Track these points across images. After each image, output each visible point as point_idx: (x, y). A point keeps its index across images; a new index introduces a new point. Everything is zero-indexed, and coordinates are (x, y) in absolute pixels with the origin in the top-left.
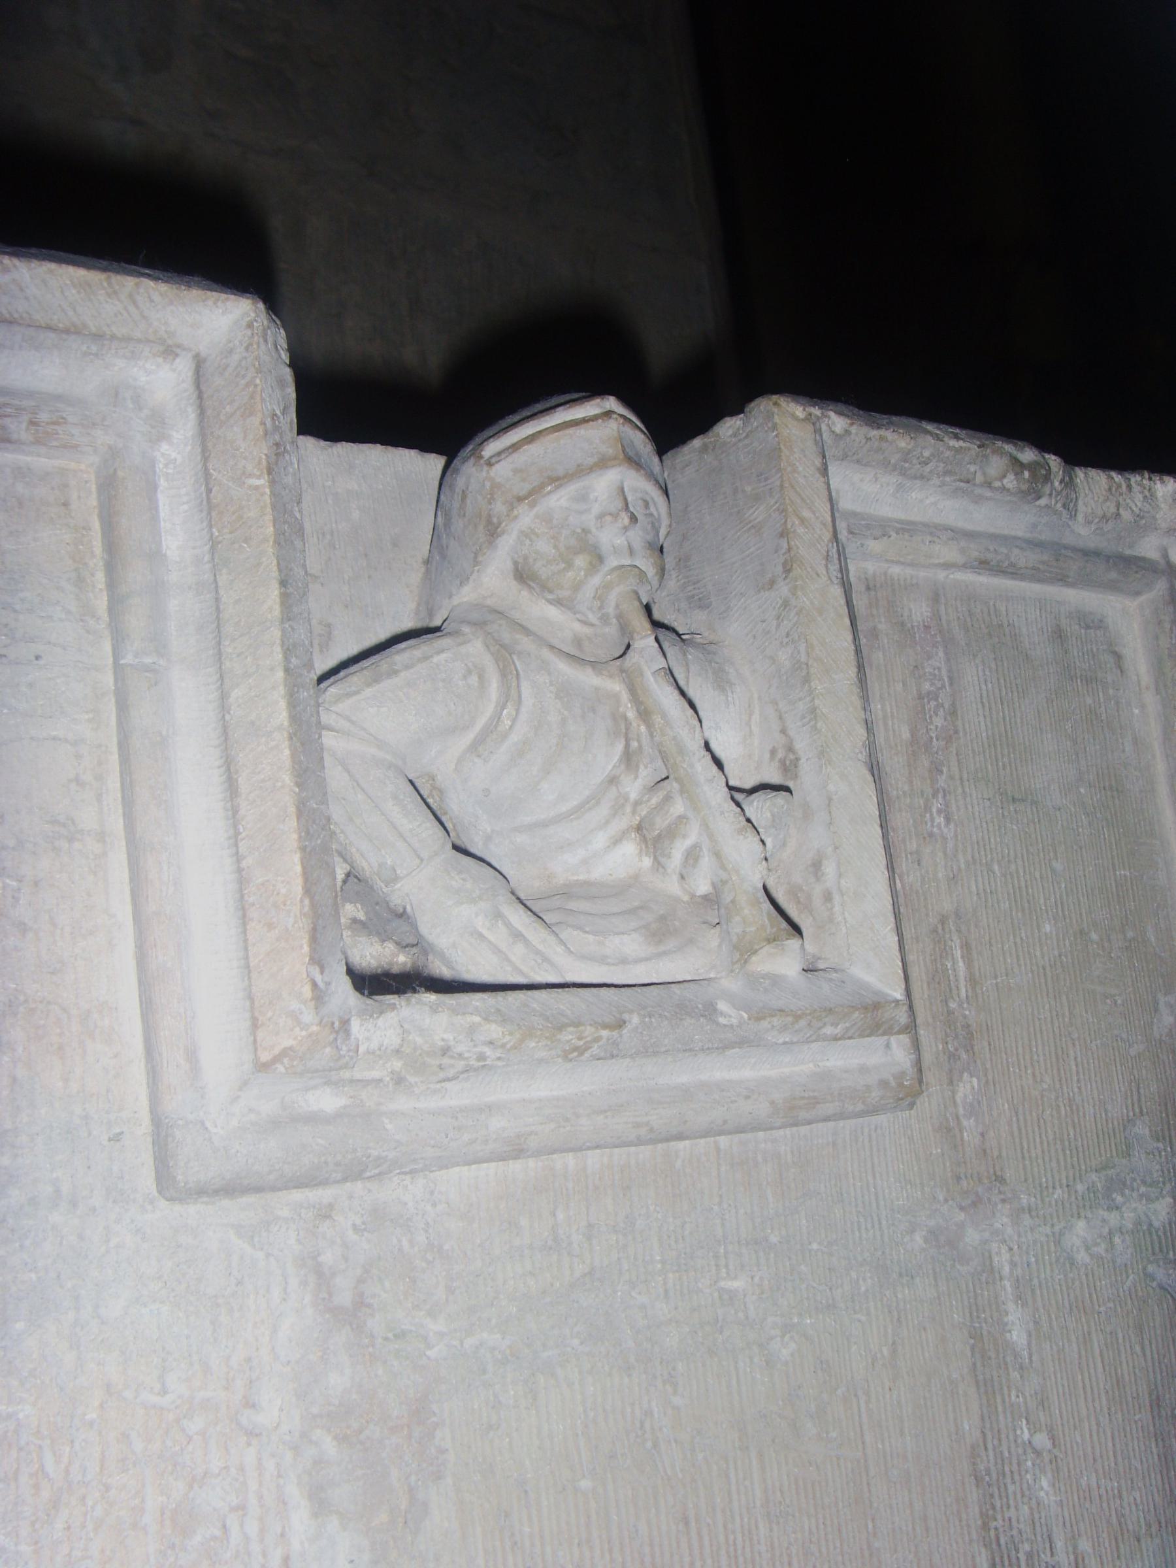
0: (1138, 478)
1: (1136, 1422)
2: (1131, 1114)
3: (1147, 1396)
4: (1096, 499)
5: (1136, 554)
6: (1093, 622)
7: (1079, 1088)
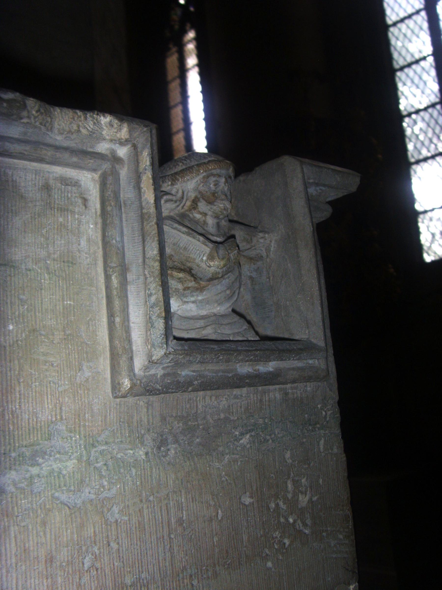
0: (92, 114)
1: (34, 570)
2: (54, 419)
3: (44, 557)
4: (65, 122)
5: (95, 151)
6: (71, 182)
7: (20, 406)
